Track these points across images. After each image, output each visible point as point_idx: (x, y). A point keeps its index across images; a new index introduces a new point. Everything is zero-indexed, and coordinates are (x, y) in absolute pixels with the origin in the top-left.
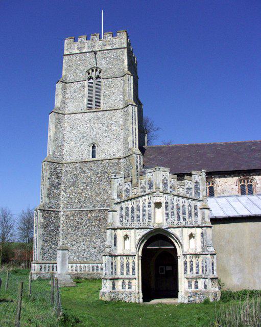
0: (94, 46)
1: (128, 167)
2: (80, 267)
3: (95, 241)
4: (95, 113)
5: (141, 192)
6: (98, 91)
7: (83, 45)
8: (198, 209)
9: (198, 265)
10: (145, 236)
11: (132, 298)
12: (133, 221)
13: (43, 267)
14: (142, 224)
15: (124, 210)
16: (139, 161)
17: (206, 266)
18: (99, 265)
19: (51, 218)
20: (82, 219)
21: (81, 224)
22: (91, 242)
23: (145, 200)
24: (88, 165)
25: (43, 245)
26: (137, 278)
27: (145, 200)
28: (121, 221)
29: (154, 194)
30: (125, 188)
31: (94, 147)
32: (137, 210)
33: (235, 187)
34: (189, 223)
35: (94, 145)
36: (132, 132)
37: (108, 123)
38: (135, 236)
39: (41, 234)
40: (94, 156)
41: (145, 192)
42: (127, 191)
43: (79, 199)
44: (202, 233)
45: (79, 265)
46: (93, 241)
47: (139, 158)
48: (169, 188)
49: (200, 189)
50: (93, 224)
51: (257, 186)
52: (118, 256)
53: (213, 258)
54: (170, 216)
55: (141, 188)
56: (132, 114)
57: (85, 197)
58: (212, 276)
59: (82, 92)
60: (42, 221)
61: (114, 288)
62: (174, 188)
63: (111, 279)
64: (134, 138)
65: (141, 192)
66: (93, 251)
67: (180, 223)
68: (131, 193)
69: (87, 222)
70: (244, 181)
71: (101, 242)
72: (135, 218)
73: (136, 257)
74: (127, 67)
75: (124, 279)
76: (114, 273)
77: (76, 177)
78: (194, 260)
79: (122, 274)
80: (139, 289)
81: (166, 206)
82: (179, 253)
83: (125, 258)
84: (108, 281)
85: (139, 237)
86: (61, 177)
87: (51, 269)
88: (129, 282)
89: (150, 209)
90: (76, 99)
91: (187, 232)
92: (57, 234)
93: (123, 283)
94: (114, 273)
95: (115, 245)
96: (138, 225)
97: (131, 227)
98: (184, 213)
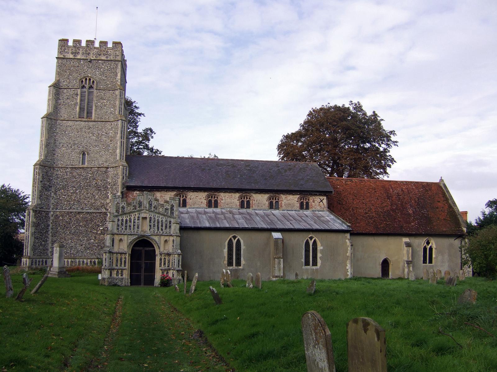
0: (89, 54)
1: (115, 176)
2: (68, 261)
3: (82, 239)
5: (133, 209)
7: (78, 51)
8: (172, 224)
9: (169, 261)
10: (134, 240)
11: (123, 282)
12: (126, 229)
13: (34, 262)
16: (125, 172)
19: (42, 218)
20: (71, 219)
21: (69, 224)
25: (34, 242)
26: (127, 269)
28: (118, 229)
29: (142, 211)
30: (122, 206)
32: (130, 222)
33: (204, 201)
34: (165, 233)
35: (84, 153)
38: (128, 240)
39: (33, 232)
40: (83, 163)
41: (136, 209)
42: (123, 207)
43: (68, 201)
44: (173, 240)
45: (67, 260)
47: (125, 170)
48: (153, 208)
49: (174, 210)
50: (80, 224)
52: (115, 253)
53: (179, 257)
54: (152, 227)
57: (74, 200)
58: (178, 269)
60: (35, 220)
61: (111, 275)
62: (157, 208)
63: (109, 269)
64: (122, 151)
68: (125, 209)
69: (75, 222)
70: (212, 197)
71: (88, 240)
72: (128, 227)
73: (127, 255)
74: (119, 81)
75: (118, 270)
76: (111, 264)
77: (66, 181)
78: (167, 258)
79: (117, 266)
80: (128, 277)
81: (150, 220)
82: (157, 252)
83: (119, 255)
85: (129, 241)
86: (52, 180)
87: (41, 263)
88: (122, 272)
89: (138, 221)
90: (69, 106)
91: (163, 239)
92: (47, 232)
93: (117, 272)
94: (111, 264)
95: (113, 246)
96: (130, 232)
97: (124, 233)
98: (162, 226)
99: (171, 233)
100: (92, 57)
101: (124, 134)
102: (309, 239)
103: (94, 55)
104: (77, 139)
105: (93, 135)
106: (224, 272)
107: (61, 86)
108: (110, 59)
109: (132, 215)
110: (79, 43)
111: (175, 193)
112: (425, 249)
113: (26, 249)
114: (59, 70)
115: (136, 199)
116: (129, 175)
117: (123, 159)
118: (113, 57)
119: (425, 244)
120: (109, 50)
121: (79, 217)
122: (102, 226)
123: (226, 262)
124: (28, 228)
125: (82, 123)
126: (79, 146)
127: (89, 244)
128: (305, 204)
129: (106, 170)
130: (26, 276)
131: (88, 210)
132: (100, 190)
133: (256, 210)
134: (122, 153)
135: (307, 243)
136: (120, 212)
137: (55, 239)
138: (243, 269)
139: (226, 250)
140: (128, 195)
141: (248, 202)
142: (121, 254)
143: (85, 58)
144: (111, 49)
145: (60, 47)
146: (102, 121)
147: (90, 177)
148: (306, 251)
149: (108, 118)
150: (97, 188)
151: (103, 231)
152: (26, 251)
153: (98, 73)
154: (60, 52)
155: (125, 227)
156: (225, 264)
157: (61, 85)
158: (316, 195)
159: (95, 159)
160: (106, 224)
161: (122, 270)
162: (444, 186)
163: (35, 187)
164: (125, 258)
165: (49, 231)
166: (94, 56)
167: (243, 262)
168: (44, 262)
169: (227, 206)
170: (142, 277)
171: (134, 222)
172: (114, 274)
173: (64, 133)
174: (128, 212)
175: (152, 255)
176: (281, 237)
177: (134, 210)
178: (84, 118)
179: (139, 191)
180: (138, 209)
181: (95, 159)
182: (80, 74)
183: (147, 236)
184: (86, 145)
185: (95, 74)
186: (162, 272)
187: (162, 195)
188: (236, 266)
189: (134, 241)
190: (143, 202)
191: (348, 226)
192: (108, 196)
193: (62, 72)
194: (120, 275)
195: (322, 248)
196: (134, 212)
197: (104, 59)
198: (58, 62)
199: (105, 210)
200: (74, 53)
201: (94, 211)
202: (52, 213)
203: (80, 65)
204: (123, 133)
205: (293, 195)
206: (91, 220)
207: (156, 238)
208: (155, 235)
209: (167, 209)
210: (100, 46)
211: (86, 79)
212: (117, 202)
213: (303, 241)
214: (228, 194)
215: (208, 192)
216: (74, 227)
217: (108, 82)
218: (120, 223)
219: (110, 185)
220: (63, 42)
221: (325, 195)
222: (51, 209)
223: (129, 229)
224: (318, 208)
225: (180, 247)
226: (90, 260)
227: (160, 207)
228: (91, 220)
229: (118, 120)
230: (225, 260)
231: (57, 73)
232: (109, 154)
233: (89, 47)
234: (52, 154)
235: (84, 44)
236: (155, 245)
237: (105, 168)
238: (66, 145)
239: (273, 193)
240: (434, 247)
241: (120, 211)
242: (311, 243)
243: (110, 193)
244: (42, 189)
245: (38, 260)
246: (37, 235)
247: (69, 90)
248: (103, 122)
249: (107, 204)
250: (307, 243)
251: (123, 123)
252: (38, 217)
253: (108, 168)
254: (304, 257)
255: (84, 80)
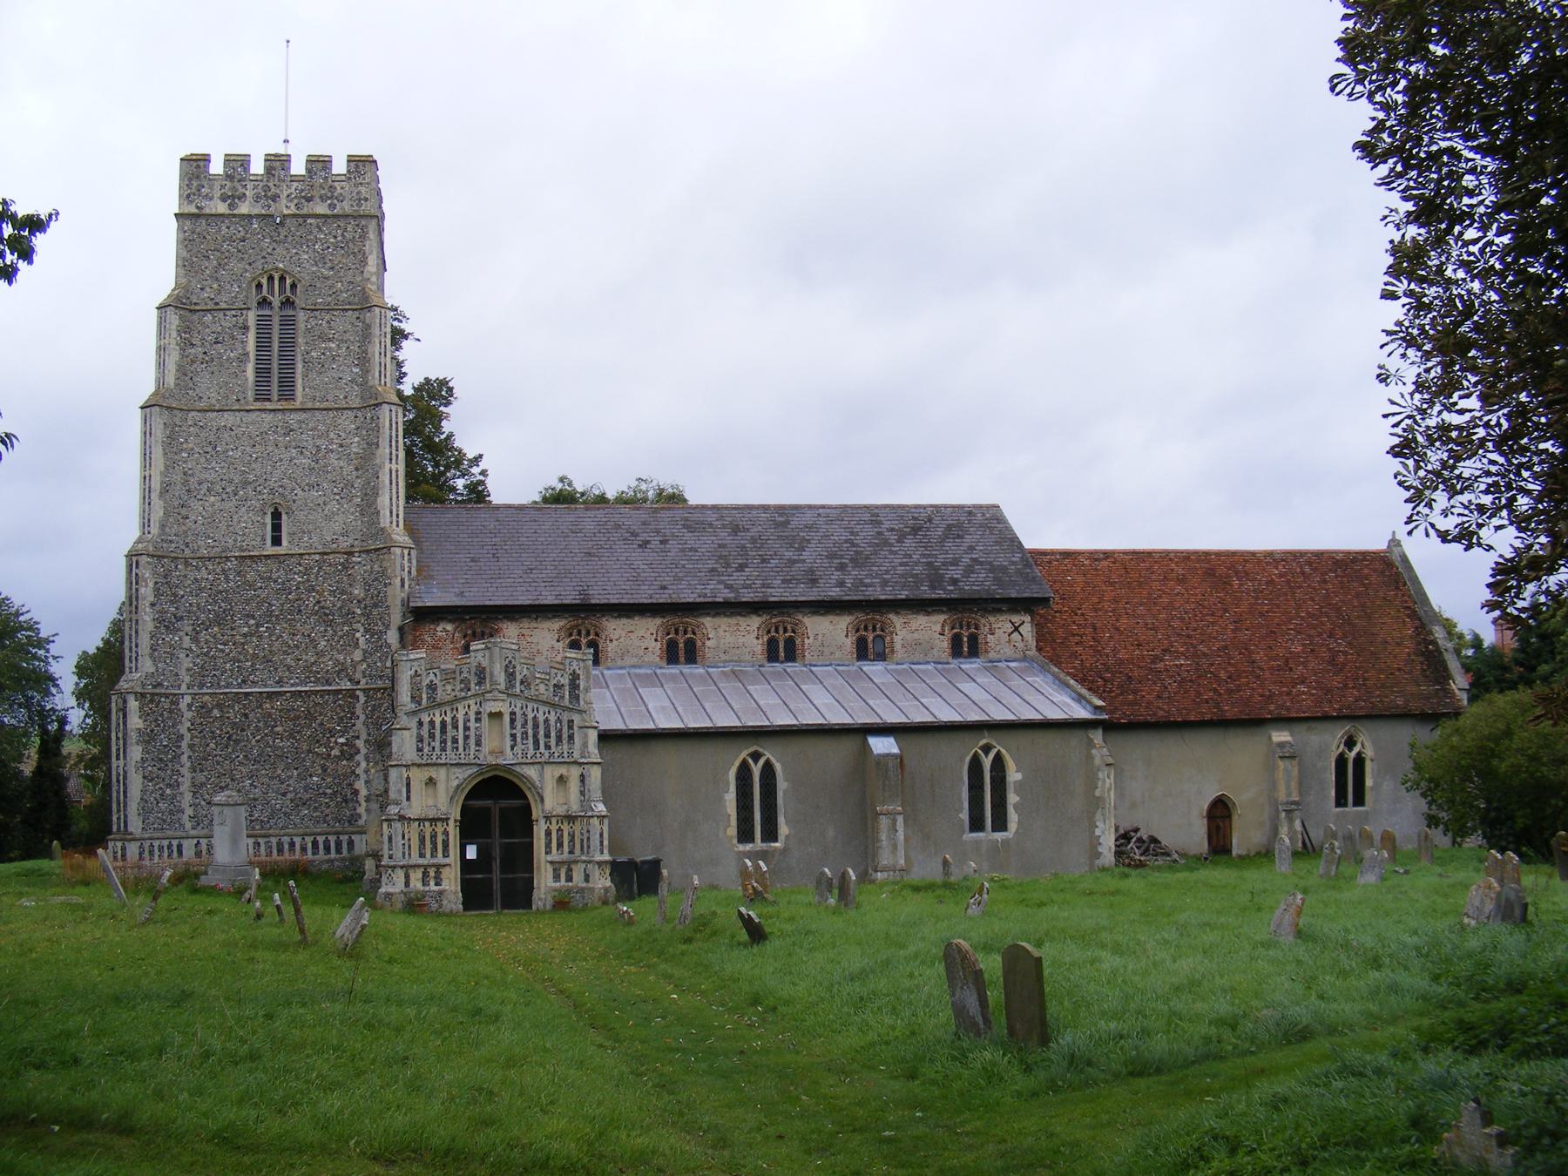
0: (275, 198)
1: (376, 579)
3: (283, 776)
4: (280, 416)
5: (461, 690)
6: (288, 344)
8: (576, 728)
12: (443, 749)
14: (462, 756)
15: (426, 727)
16: (407, 564)
17: (588, 839)
18: (295, 839)
19: (162, 715)
20: (246, 716)
21: (243, 730)
22: (272, 778)
23: (469, 706)
24: (261, 568)
25: (144, 791)
27: (469, 706)
28: (420, 750)
29: (488, 696)
30: (428, 681)
31: (277, 516)
32: (453, 727)
33: (654, 643)
34: (556, 755)
35: (276, 509)
36: (387, 482)
37: (319, 449)
39: (139, 759)
40: (277, 541)
41: (469, 690)
42: (432, 687)
43: (235, 660)
46: (279, 776)
47: (406, 558)
48: (518, 684)
49: (581, 687)
50: (276, 729)
51: (708, 643)
53: (601, 823)
54: (519, 739)
55: (462, 681)
56: (391, 429)
59: (238, 345)
61: (407, 884)
64: (394, 500)
65: (461, 690)
66: (277, 803)
67: (538, 755)
68: (439, 691)
69: (261, 725)
71: (301, 778)
72: (449, 744)
73: (451, 823)
75: (426, 867)
78: (566, 828)
81: (511, 719)
84: (396, 870)
85: (455, 783)
87: (166, 854)
88: (438, 873)
89: (477, 725)
91: (551, 773)
92: (177, 757)
93: (425, 875)
95: (408, 799)
96: (454, 757)
97: (439, 761)
98: (547, 736)
99: (576, 755)
100: (285, 207)
101: (397, 447)
102: (980, 751)
103: (291, 201)
104: (253, 466)
105: (302, 452)
106: (747, 867)
107: (195, 304)
108: (340, 213)
109: (460, 708)
110: (242, 165)
111: (562, 623)
112: (1341, 762)
113: (119, 811)
114: (185, 254)
115: (468, 661)
116: (417, 571)
117: (398, 525)
118: (352, 205)
119: (1342, 746)
120: (336, 184)
121: (273, 707)
122: (343, 733)
123: (732, 831)
124: (122, 750)
125: (264, 415)
126: (259, 489)
127: (306, 788)
128: (965, 639)
129: (347, 560)
130: (281, 899)
131: (297, 685)
132: (330, 623)
133: (815, 666)
134: (394, 505)
135: (975, 765)
136: (424, 701)
137: (201, 778)
138: (785, 850)
139: (731, 797)
140: (420, 635)
141: (790, 644)
142: (433, 821)
143: (263, 212)
144: (343, 178)
145: (187, 182)
146: (325, 409)
147: (299, 582)
148: (971, 788)
149: (346, 397)
150: (320, 617)
151: (345, 748)
152: (119, 819)
153: (306, 257)
154: (187, 196)
155: (441, 743)
156: (731, 837)
157: (195, 301)
158: (1000, 611)
159: (310, 527)
160: (354, 725)
161: (438, 867)
162: (1402, 560)
163: (134, 622)
164: (446, 833)
165: (183, 753)
166: (293, 207)
167: (783, 830)
168: (175, 849)
169: (724, 657)
170: (497, 886)
171: (467, 728)
172: (416, 883)
173: (209, 449)
174: (448, 698)
175: (521, 821)
176: (896, 750)
177: (463, 694)
178: (269, 400)
179: (450, 621)
180: (474, 688)
181: (310, 527)
182: (250, 264)
183: (507, 768)
184: (281, 486)
185: (300, 262)
186: (555, 870)
187: (524, 631)
188: (762, 841)
189: (470, 782)
190: (488, 670)
191: (1097, 708)
192: (358, 640)
193: (195, 259)
194: (432, 883)
195: (1019, 776)
196: (464, 698)
197: (322, 212)
198: (181, 229)
199: (349, 683)
200: (229, 197)
201: (317, 688)
202: (188, 699)
203: (248, 236)
204: (394, 444)
205: (928, 614)
206: (310, 716)
207: (531, 772)
208: (526, 764)
209: (558, 686)
210: (309, 171)
211: (271, 278)
212: (413, 672)
213: (962, 759)
214: (725, 619)
215: (664, 617)
216: (257, 738)
217: (339, 285)
218: (425, 732)
219: (362, 606)
220: (194, 166)
221: (1028, 611)
222: (184, 688)
223: (453, 748)
224: (1006, 650)
225: (603, 793)
226: (312, 838)
227: (538, 681)
228: (310, 716)
229: (377, 405)
230: (729, 826)
231: (179, 263)
232: (352, 510)
233: (274, 175)
234: (179, 517)
235: (257, 167)
236: (530, 797)
237: (344, 553)
238: (218, 488)
239: (864, 611)
240: (1369, 753)
241: (424, 696)
242: (987, 762)
243: (362, 630)
244: (156, 627)
245: (156, 843)
246: (150, 768)
247: (221, 315)
248: (331, 409)
249: (354, 665)
250: (975, 765)
251: (394, 413)
252: (148, 715)
253: (351, 554)
254: (966, 805)
255: (264, 281)
